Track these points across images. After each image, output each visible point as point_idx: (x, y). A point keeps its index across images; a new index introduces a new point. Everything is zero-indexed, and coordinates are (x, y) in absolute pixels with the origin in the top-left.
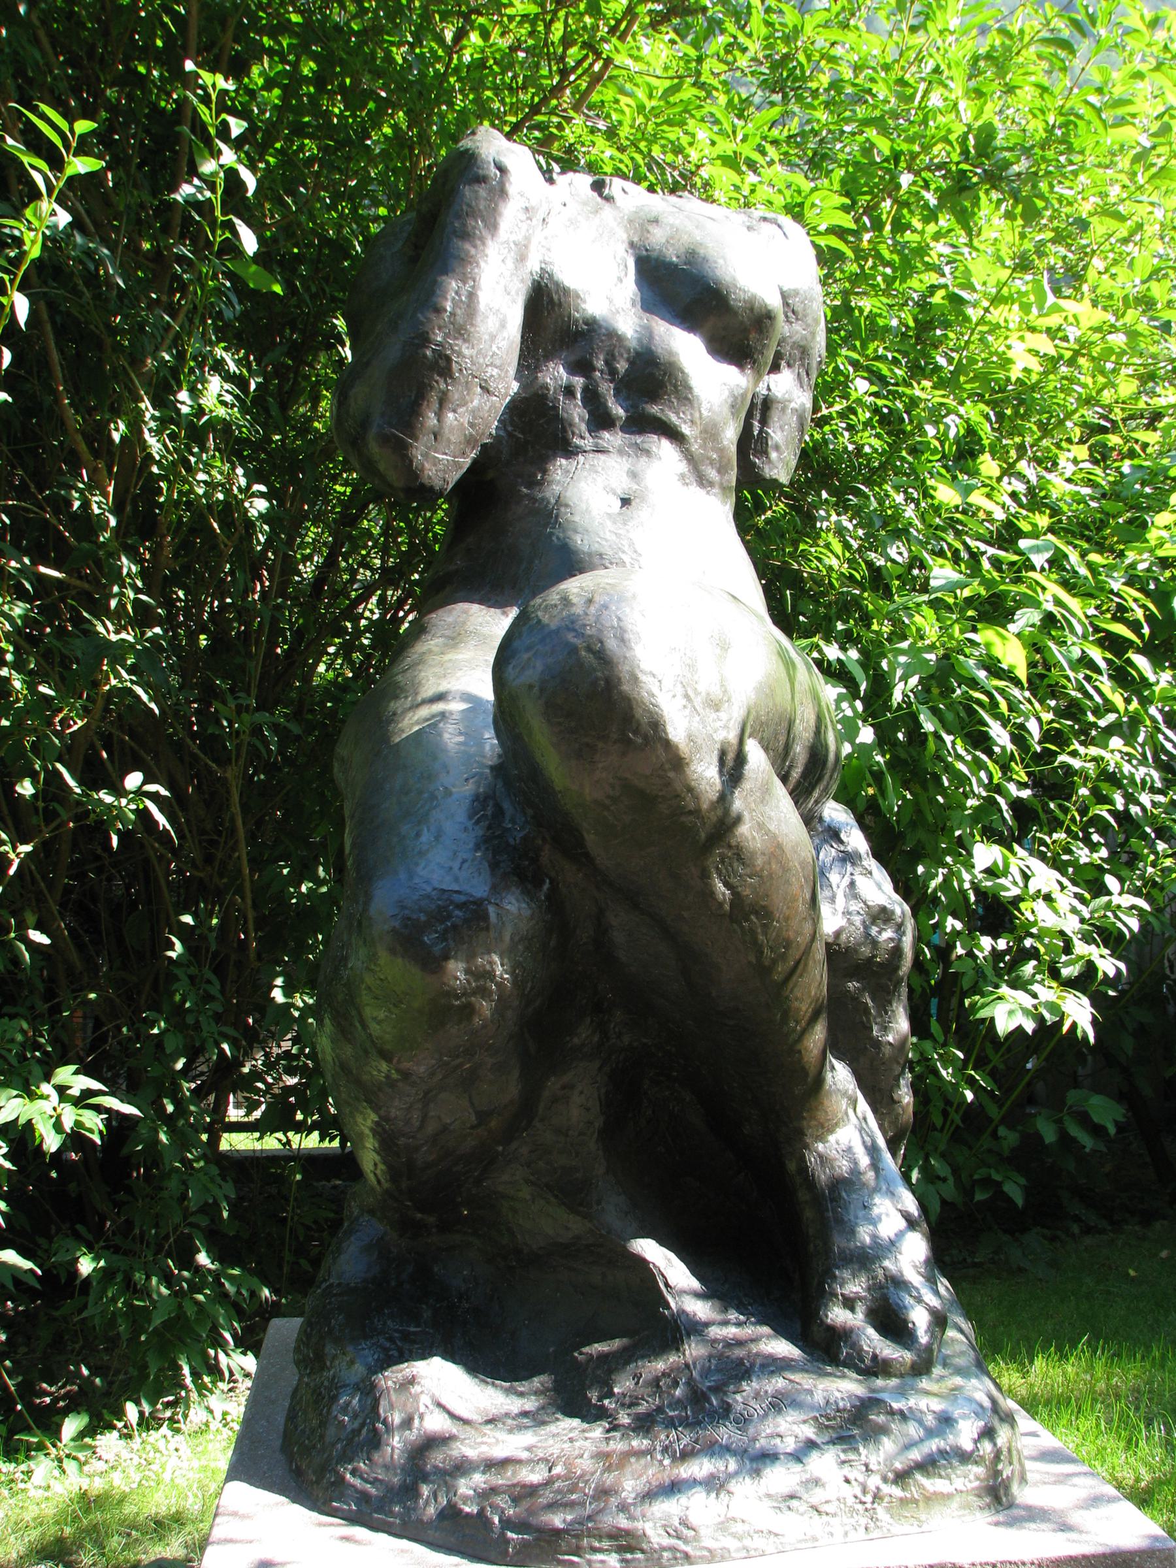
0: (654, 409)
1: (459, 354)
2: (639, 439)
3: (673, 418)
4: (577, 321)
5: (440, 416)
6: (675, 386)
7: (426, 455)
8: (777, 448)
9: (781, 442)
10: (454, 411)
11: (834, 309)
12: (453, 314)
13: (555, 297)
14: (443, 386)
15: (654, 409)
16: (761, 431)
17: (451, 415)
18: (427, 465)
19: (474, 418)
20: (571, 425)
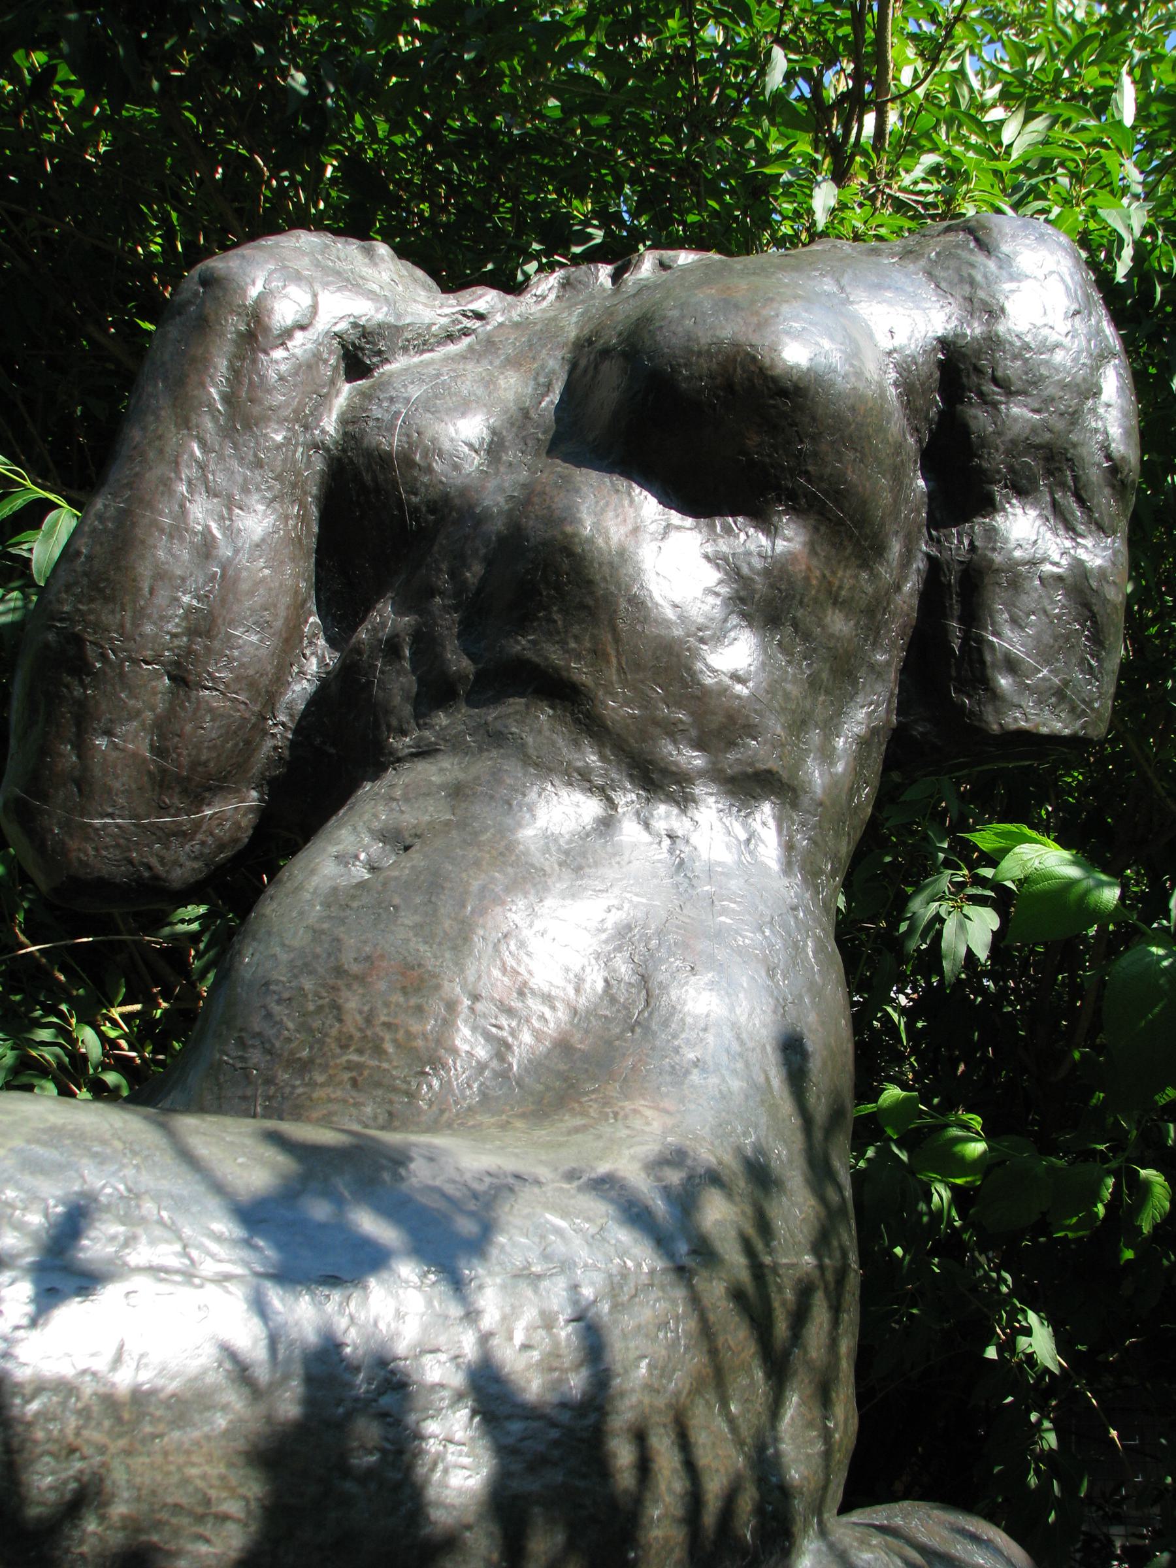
0: (521, 645)
1: (98, 627)
2: (491, 714)
3: (555, 655)
4: (415, 510)
5: (81, 747)
6: (558, 587)
7: (66, 825)
8: (1012, 665)
9: (1018, 651)
10: (109, 733)
11: (709, 350)
12: (90, 558)
13: (367, 478)
14: (78, 692)
15: (521, 645)
16: (966, 639)
17: (102, 742)
18: (73, 844)
19: (162, 736)
20: (388, 712)
